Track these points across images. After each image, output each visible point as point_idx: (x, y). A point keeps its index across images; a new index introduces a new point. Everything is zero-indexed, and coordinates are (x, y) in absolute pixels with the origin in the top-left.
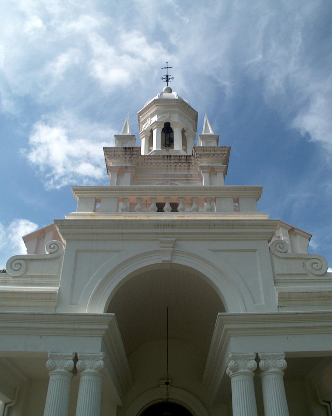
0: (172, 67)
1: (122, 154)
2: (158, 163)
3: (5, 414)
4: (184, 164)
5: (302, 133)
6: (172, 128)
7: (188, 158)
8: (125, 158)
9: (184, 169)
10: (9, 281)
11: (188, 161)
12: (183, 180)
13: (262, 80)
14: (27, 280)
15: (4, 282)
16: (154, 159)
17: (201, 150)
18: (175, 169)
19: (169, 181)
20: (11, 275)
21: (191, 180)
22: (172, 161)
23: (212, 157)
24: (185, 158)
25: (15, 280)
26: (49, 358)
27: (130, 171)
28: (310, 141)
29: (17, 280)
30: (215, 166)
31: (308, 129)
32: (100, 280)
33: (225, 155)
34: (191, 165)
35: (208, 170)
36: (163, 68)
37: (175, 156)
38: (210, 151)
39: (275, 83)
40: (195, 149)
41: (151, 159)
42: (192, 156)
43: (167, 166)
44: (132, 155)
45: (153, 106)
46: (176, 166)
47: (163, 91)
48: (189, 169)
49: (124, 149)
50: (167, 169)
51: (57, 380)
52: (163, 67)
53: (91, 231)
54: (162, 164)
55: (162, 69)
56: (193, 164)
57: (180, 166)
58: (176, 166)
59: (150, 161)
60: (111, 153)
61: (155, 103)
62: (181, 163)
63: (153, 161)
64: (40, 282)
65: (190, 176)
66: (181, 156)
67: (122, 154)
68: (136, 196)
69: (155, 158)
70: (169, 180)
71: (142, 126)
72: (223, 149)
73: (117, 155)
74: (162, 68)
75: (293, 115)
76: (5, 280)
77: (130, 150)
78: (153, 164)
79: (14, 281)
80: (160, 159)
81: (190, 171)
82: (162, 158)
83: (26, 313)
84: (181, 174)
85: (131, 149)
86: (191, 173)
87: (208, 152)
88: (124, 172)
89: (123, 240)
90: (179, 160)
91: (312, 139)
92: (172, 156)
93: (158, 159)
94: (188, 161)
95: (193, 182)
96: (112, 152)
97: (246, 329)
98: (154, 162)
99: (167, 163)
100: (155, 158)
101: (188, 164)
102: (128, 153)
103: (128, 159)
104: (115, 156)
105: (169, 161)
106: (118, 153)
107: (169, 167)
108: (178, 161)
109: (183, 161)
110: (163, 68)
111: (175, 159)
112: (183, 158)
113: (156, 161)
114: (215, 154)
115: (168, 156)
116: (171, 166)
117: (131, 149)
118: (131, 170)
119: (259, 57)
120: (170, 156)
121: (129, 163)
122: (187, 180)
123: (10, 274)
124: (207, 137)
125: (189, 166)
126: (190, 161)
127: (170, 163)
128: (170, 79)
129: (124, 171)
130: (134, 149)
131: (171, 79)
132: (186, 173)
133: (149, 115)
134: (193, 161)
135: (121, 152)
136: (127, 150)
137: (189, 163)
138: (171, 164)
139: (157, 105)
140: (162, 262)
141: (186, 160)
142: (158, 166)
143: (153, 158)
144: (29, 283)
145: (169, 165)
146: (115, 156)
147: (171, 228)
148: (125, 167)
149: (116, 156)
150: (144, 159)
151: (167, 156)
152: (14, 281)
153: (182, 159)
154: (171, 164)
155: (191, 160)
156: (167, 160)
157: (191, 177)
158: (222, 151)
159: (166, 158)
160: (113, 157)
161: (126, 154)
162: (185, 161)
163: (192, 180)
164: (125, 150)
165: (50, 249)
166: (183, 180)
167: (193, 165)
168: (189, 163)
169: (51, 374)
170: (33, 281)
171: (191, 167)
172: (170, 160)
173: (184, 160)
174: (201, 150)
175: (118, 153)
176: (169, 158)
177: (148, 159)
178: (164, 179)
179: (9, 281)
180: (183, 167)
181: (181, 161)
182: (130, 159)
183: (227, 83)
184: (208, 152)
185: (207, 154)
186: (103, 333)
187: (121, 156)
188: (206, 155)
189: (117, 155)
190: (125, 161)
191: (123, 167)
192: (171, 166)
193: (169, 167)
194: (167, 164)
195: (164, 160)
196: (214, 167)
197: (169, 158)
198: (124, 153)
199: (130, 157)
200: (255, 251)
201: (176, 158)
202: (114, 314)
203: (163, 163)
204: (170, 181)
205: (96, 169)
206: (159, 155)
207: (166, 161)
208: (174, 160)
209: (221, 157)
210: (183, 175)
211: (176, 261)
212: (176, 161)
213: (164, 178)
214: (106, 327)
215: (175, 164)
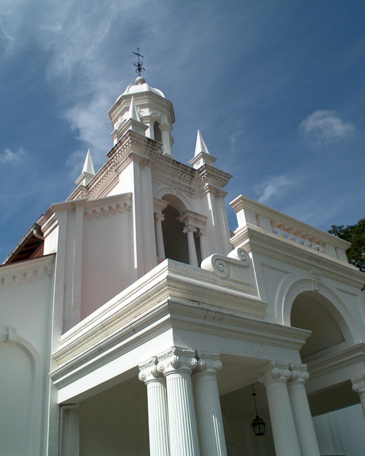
0: (143, 57)
1: (144, 145)
2: (167, 165)
4: (189, 176)
5: (73, 128)
6: (160, 129)
7: (193, 171)
8: (147, 149)
9: (187, 181)
10: (218, 281)
11: (192, 174)
12: (186, 192)
13: (51, 53)
14: (233, 284)
15: (213, 281)
16: (165, 160)
17: (210, 169)
18: (180, 177)
19: (177, 188)
20: (218, 275)
21: (193, 194)
23: (217, 180)
24: (191, 170)
25: (223, 281)
26: (274, 366)
27: (151, 165)
28: (78, 139)
29: (233, 284)
30: (219, 190)
31: (80, 125)
32: (284, 297)
34: (193, 179)
35: (213, 191)
36: (134, 53)
37: (184, 165)
38: (217, 173)
39: (64, 63)
40: (206, 166)
41: (163, 159)
42: (197, 171)
43: (174, 172)
44: (154, 149)
45: (145, 97)
48: (191, 182)
49: (148, 139)
50: (173, 175)
51: (154, 388)
52: (135, 52)
53: (271, 248)
54: (171, 169)
55: (133, 53)
56: (196, 179)
57: (185, 176)
59: (161, 160)
60: (134, 138)
61: (147, 95)
62: (186, 173)
63: (163, 162)
64: (242, 289)
65: (193, 189)
66: (188, 167)
67: (144, 145)
68: (282, 222)
69: (167, 159)
70: (177, 187)
71: (125, 112)
72: (227, 176)
73: (140, 143)
74: (134, 52)
75: (70, 104)
76: (215, 280)
77: (153, 143)
78: (163, 165)
79: (222, 282)
80: (170, 162)
81: (191, 185)
82: (172, 162)
83: (257, 320)
84: (186, 185)
85: (154, 143)
86: (192, 187)
87: (215, 174)
88: (145, 164)
89: (288, 263)
90: (185, 170)
91: (81, 137)
92: (181, 163)
93: (168, 162)
94: (192, 174)
95: (193, 196)
96: (135, 137)
97: (134, 347)
98: (164, 164)
99: (175, 169)
100: (167, 159)
101: (192, 177)
102: (150, 145)
103: (148, 152)
104: (138, 143)
105: (177, 168)
106: (141, 141)
107: (176, 174)
108: (184, 171)
109: (188, 173)
111: (182, 168)
112: (189, 169)
113: (166, 163)
114: (220, 177)
115: (178, 163)
116: (178, 173)
117: (154, 143)
118: (152, 165)
119: (58, 28)
120: (179, 163)
121: (148, 156)
122: (190, 193)
123: (217, 274)
124: (208, 156)
125: (192, 179)
126: (194, 175)
127: (178, 170)
128: (142, 69)
129: (145, 163)
130: (156, 144)
131: (143, 70)
132: (188, 185)
133: (139, 104)
134: (196, 176)
135: (144, 141)
136: (150, 142)
137: (192, 176)
138: (178, 172)
139: (149, 98)
140: (313, 290)
141: (191, 173)
142: (167, 168)
143: (164, 158)
144: (233, 287)
145: (176, 172)
146: (138, 143)
147: (317, 262)
148: (147, 159)
149: (139, 144)
150: (157, 157)
151: (177, 162)
152: (222, 282)
153: (188, 171)
155: (195, 174)
156: (176, 166)
157: (193, 191)
158: (225, 177)
159: (175, 163)
160: (136, 144)
161: (148, 146)
162: (190, 173)
163: (194, 194)
164: (148, 141)
166: (186, 192)
167: (195, 180)
168: (192, 176)
169: (147, 383)
170: (238, 286)
171: (193, 181)
172: (178, 167)
173: (190, 172)
174: (210, 169)
175: (141, 141)
176: (178, 164)
177: (160, 158)
178: (171, 185)
179: (218, 281)
180: (187, 179)
181: (186, 172)
182: (150, 152)
183: (11, 39)
184: (215, 174)
185: (214, 175)
186: (301, 347)
187: (144, 146)
188: (213, 176)
189: (140, 143)
190: (145, 153)
191: (146, 159)
193: (176, 174)
194: (174, 170)
195: (173, 164)
196: (219, 190)
198: (146, 144)
199: (151, 151)
200: (356, 295)
201: (184, 167)
202: (311, 332)
203: (172, 167)
204: (178, 189)
206: (170, 158)
207: (174, 166)
208: (181, 168)
209: (223, 183)
210: (188, 187)
211: (319, 292)
213: (172, 183)
214: (304, 342)
215: (182, 173)
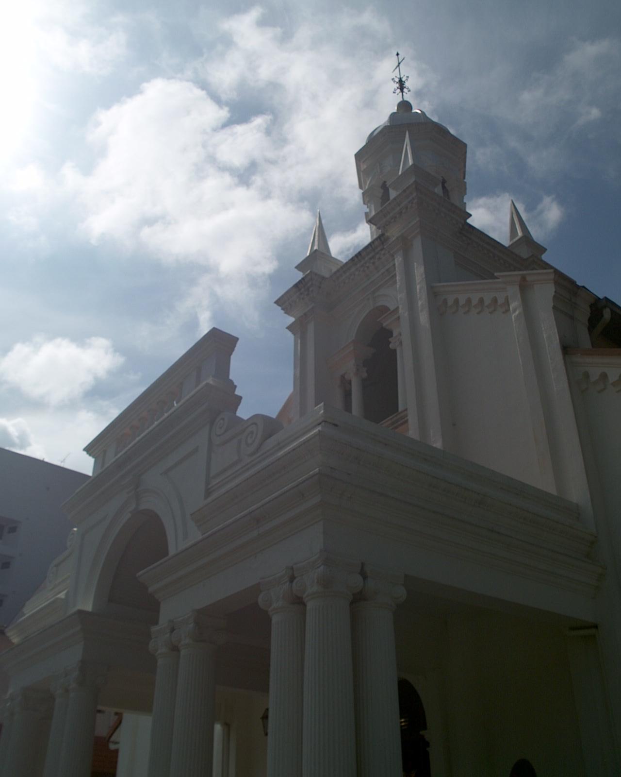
3: (232, 772)
7: (382, 239)
8: (303, 299)
22: (367, 259)
33: (415, 201)
46: (374, 263)
47: (415, 109)
55: (394, 72)
57: (379, 258)
58: (374, 263)
62: (378, 253)
110: (394, 70)
116: (368, 267)
138: (368, 265)
154: (368, 265)
159: (356, 259)
161: (301, 294)
165: (379, 424)
192: (368, 267)
197: (359, 257)
205: (44, 459)
212: (371, 255)
215: (372, 261)
